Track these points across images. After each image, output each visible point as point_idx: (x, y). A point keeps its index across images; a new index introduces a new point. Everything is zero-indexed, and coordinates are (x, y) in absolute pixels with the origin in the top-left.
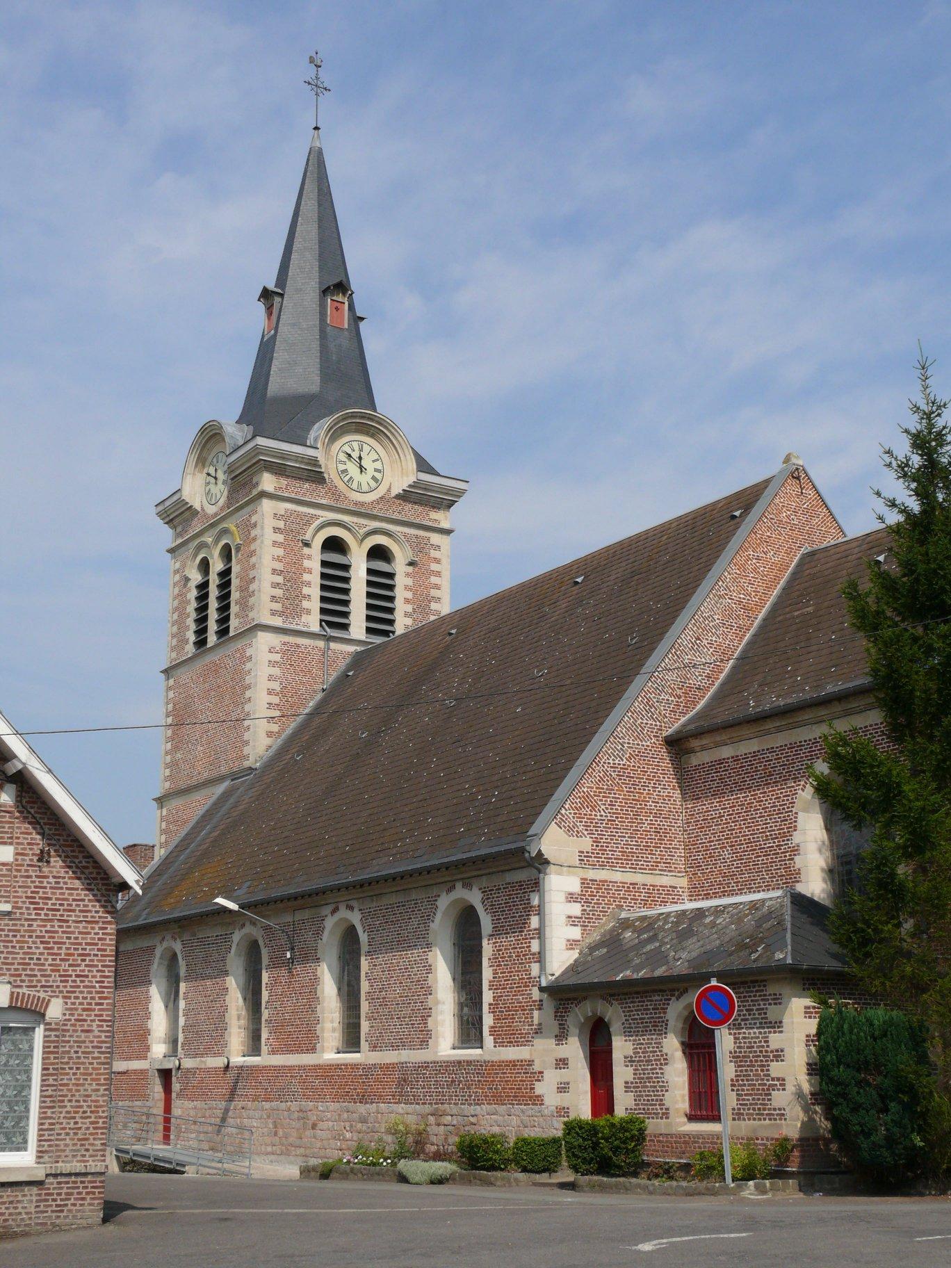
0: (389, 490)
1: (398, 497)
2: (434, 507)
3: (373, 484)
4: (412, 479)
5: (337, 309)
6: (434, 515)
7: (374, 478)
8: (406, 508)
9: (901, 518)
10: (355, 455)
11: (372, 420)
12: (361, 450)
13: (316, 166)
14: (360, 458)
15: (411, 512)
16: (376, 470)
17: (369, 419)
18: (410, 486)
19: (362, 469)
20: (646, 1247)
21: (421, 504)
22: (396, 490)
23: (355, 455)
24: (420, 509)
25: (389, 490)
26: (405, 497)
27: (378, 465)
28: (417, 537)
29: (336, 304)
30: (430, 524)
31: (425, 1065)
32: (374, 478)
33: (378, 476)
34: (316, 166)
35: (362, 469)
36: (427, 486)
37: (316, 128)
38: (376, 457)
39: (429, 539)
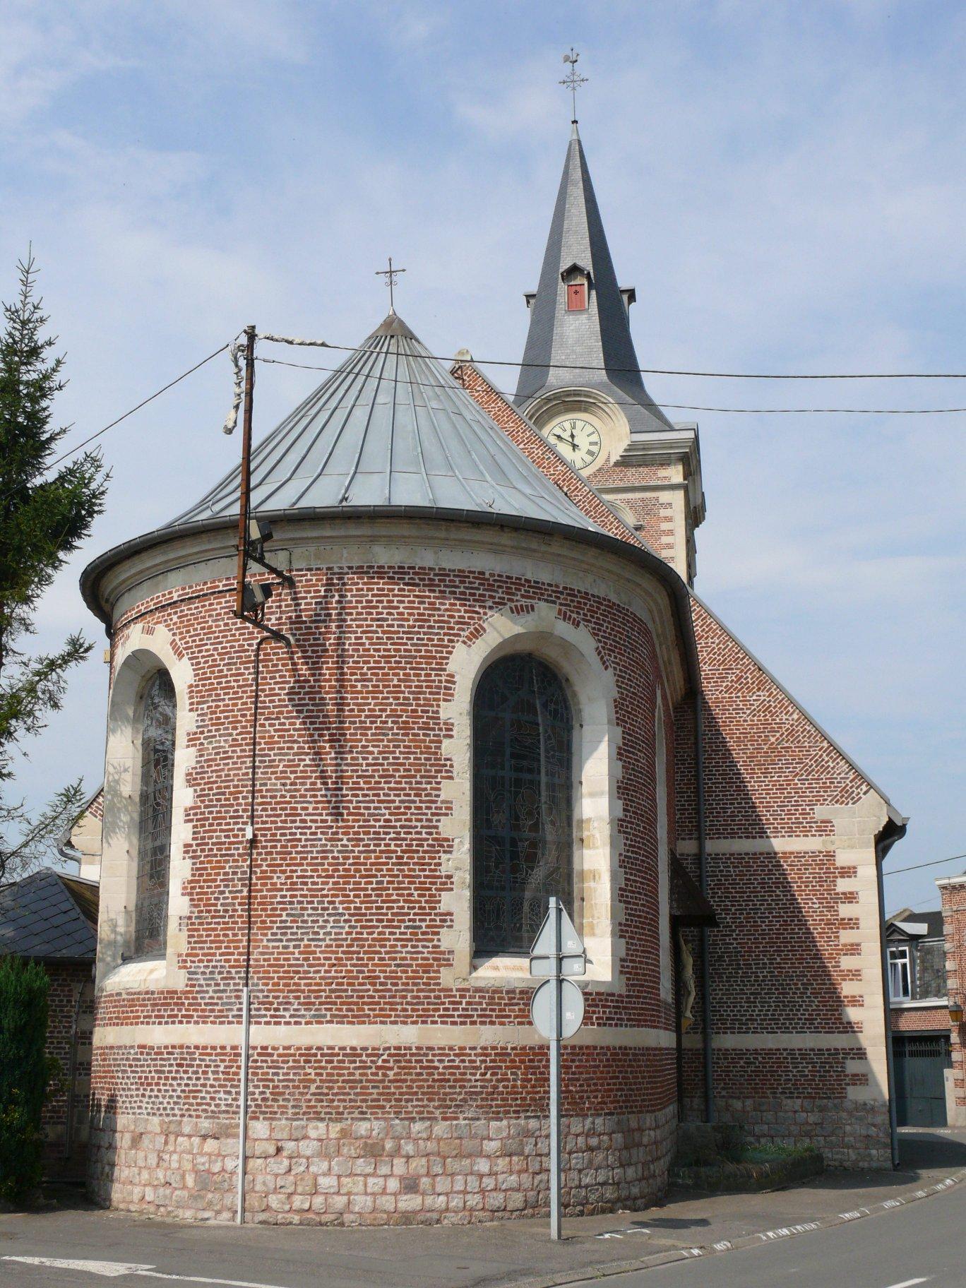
0: (608, 460)
1: (617, 464)
2: (662, 465)
3: (588, 458)
4: (625, 444)
5: (576, 292)
6: (662, 473)
7: (590, 453)
8: (629, 474)
9: (44, 437)
10: (566, 435)
11: (579, 395)
12: (574, 428)
13: (578, 157)
14: (572, 436)
15: (633, 476)
16: (591, 444)
17: (586, 396)
18: (626, 450)
19: (574, 447)
20: (847, 1216)
21: (647, 466)
22: (615, 458)
23: (566, 435)
24: (646, 470)
25: (608, 460)
26: (625, 462)
27: (594, 438)
28: (643, 500)
29: (574, 288)
30: (659, 483)
31: (755, 856)
32: (590, 453)
33: (595, 449)
34: (578, 157)
35: (574, 447)
36: (645, 446)
37: (575, 122)
38: (592, 430)
39: (657, 499)
